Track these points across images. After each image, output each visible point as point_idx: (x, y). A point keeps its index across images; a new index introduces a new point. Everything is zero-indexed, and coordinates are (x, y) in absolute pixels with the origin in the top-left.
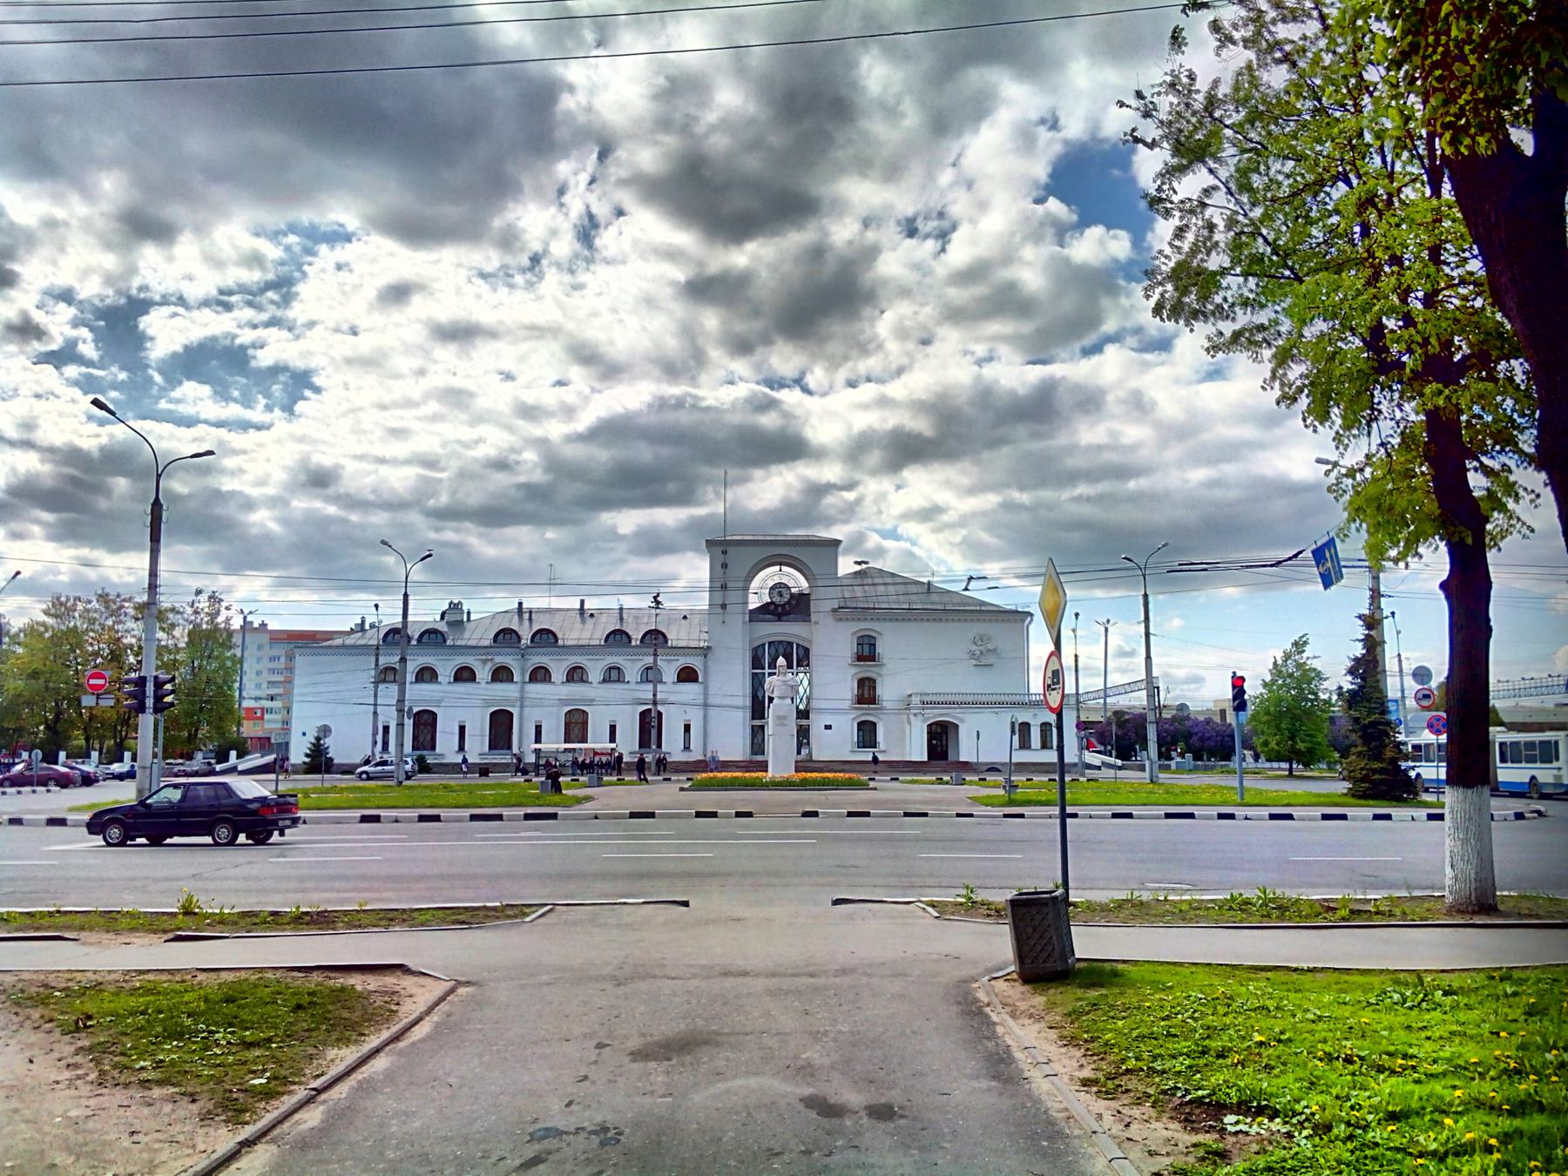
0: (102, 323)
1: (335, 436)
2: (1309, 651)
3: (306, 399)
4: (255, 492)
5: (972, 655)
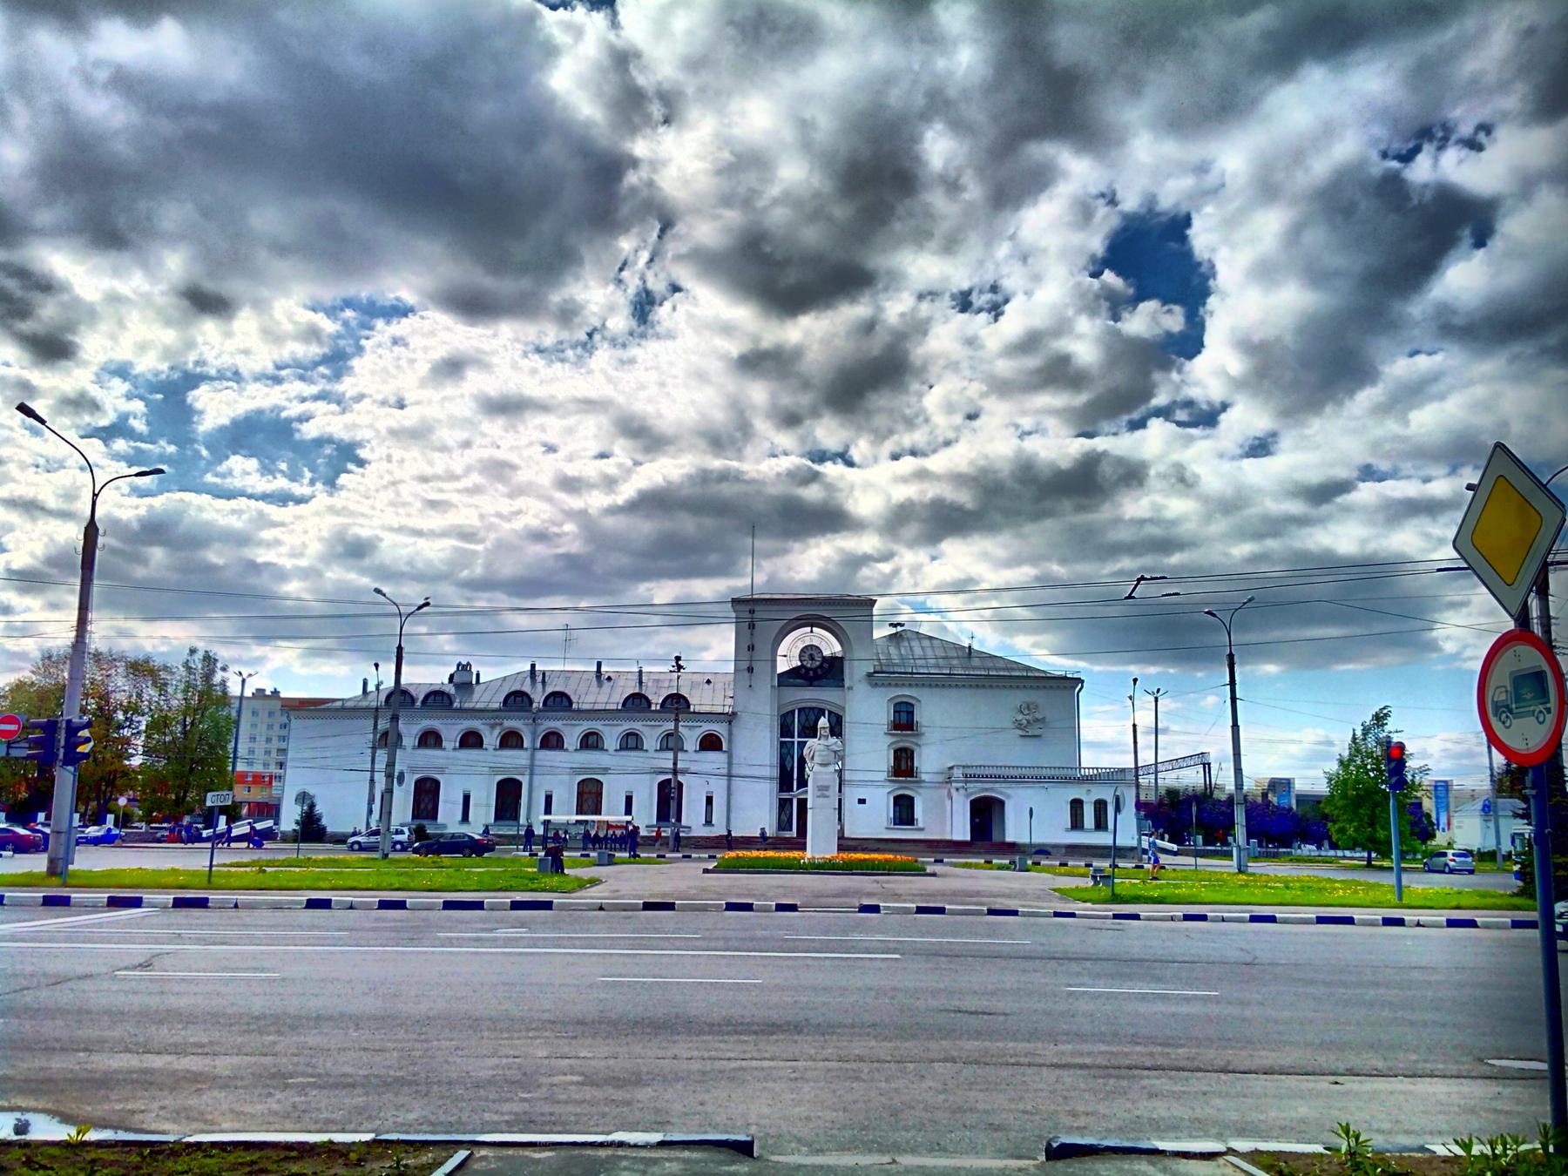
0: (160, 396)
1: (373, 508)
2: (1391, 725)
3: (348, 472)
4: (288, 563)
5: (1019, 726)
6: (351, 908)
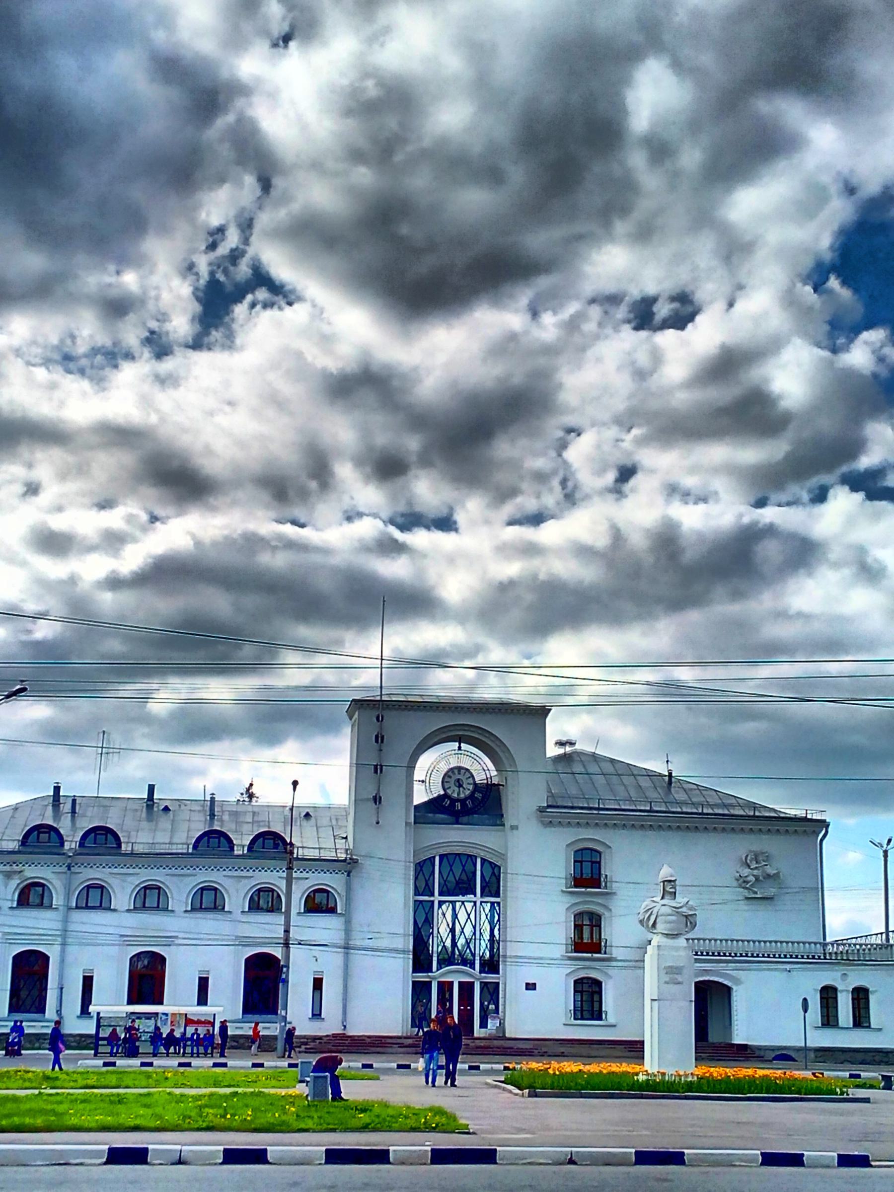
5: (743, 882)
6: (180, 1162)
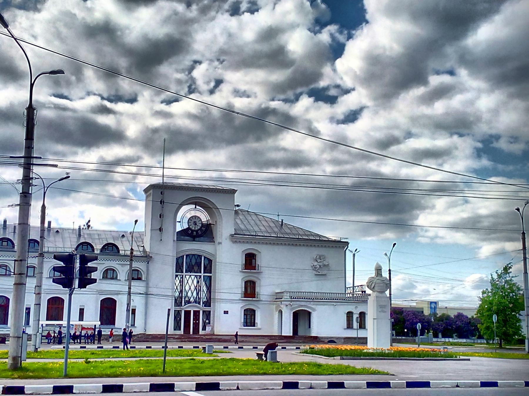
5: (314, 268)
6: (311, 388)
